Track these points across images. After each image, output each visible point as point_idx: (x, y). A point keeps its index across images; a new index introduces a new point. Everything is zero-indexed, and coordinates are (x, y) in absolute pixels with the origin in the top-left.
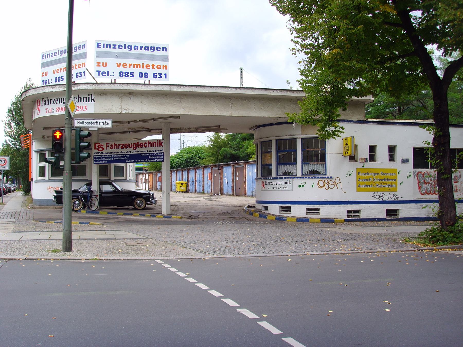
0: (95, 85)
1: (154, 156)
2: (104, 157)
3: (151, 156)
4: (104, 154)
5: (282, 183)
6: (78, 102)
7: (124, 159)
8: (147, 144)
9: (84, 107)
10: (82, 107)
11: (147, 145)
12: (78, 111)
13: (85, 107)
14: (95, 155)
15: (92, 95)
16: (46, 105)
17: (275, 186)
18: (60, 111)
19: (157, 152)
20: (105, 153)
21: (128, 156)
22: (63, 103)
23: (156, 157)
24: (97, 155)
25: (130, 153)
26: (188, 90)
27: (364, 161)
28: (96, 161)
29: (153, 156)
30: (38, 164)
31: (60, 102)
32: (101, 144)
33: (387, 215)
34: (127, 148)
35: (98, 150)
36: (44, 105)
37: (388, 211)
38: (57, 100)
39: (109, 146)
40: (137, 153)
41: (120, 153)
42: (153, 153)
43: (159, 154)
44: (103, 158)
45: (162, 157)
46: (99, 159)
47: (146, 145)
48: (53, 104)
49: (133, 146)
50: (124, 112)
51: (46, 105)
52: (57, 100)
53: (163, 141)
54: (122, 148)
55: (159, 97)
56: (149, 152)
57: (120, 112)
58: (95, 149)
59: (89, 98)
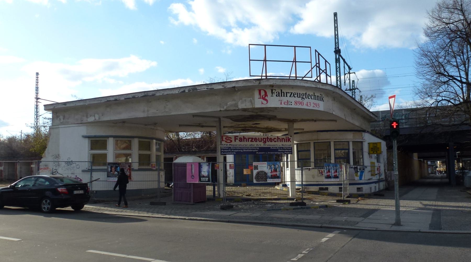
1: (283, 149)
2: (233, 148)
3: (281, 149)
4: (233, 146)
5: (313, 97)
6: (314, 99)
11: (277, 140)
14: (222, 146)
16: (279, 96)
19: (286, 146)
21: (258, 148)
22: (301, 98)
23: (285, 151)
24: (225, 146)
25: (260, 146)
29: (282, 149)
31: (299, 96)
35: (226, 142)
39: (237, 139)
40: (267, 146)
41: (250, 145)
42: (282, 147)
43: (287, 148)
44: (231, 149)
45: (291, 150)
46: (227, 151)
48: (290, 96)
51: (279, 96)
53: (291, 138)
54: (251, 141)
56: (278, 146)
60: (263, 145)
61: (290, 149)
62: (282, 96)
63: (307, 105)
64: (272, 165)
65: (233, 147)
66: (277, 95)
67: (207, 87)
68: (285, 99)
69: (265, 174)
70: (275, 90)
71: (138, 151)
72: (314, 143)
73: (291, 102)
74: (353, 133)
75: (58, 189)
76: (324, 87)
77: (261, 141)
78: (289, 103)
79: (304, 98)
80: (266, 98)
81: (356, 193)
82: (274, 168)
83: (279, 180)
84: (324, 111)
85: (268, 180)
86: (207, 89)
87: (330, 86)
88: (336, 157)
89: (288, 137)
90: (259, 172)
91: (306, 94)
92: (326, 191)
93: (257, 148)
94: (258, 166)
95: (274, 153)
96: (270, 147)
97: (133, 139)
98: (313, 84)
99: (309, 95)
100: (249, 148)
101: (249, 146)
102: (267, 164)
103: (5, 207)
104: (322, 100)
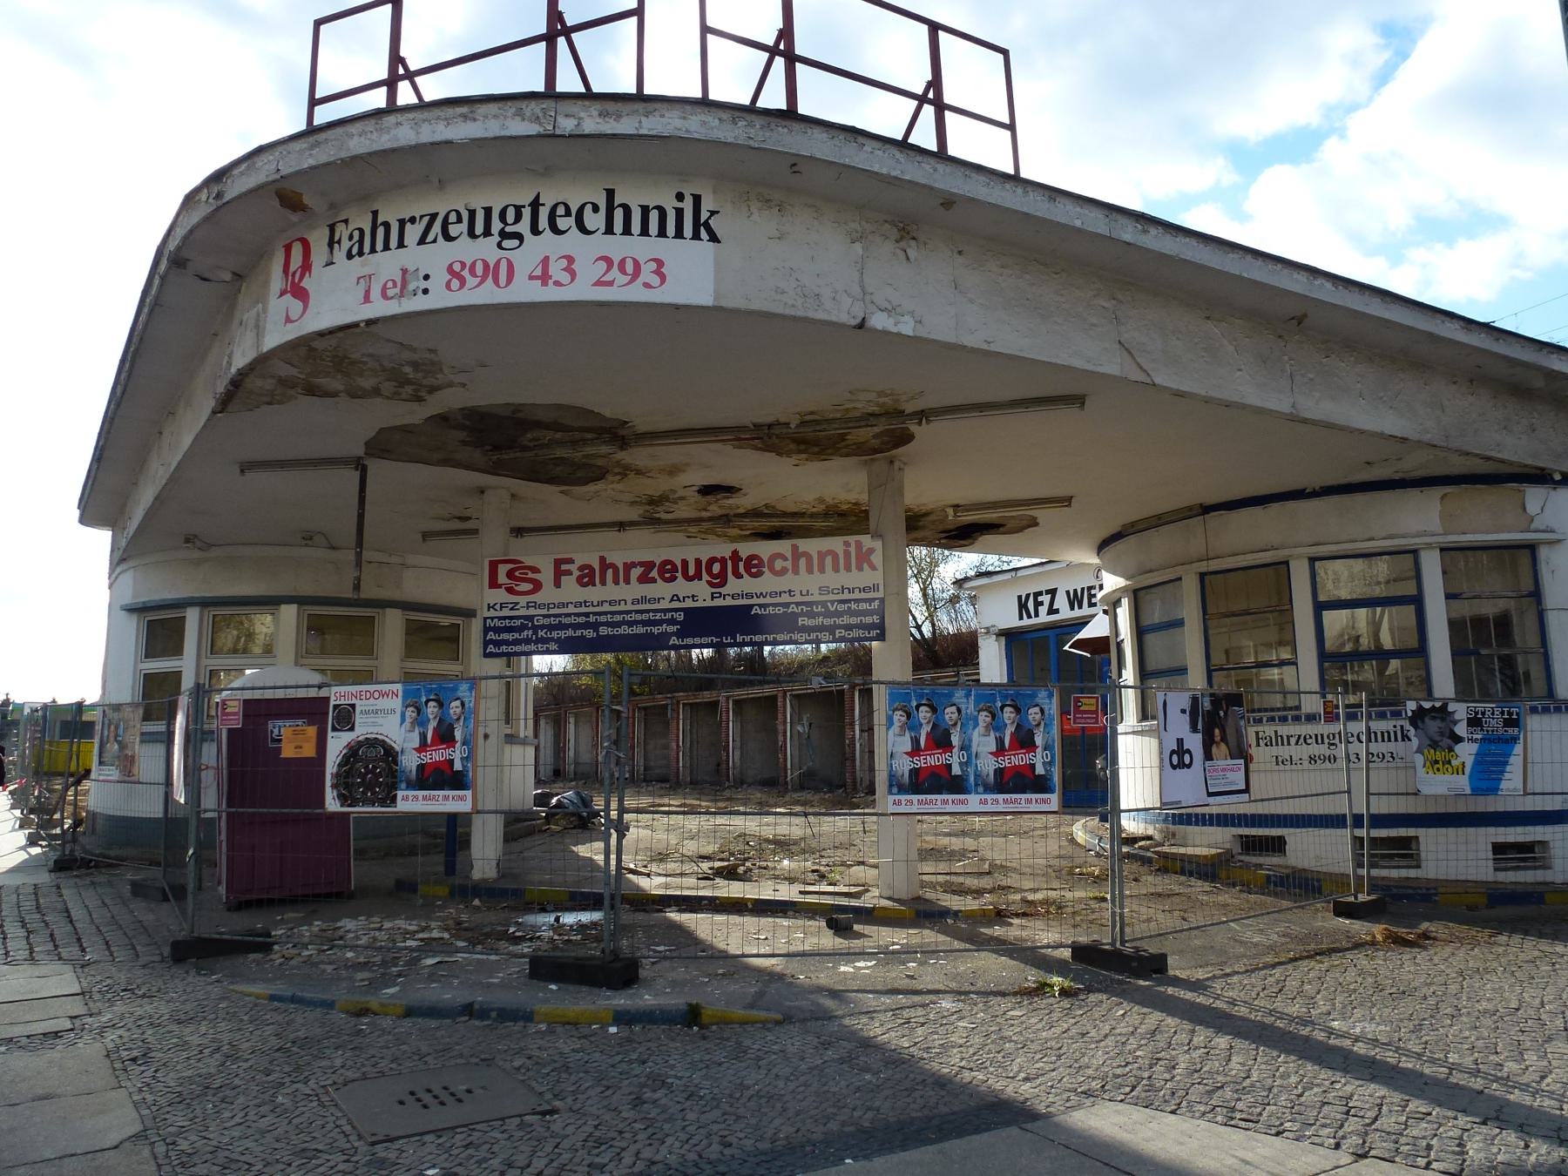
0: (750, 125)
1: (827, 614)
2: (546, 621)
3: (811, 615)
4: (545, 612)
5: (595, 221)
6: (609, 230)
7: (655, 630)
8: (785, 559)
10: (637, 264)
11: (789, 564)
12: (610, 284)
13: (564, 263)
14: (492, 613)
15: (697, 200)
16: (361, 253)
17: (1323, 750)
18: (471, 281)
21: (680, 617)
23: (839, 621)
24: (506, 612)
25: (689, 604)
28: (497, 643)
29: (819, 614)
30: (205, 662)
31: (479, 229)
32: (528, 561)
34: (673, 579)
35: (510, 590)
36: (350, 256)
38: (453, 218)
39: (569, 573)
40: (729, 602)
41: (636, 601)
42: (824, 604)
43: (853, 606)
44: (535, 629)
46: (517, 635)
47: (779, 564)
48: (422, 241)
49: (709, 571)
51: (361, 253)
52: (453, 218)
54: (645, 579)
56: (798, 598)
57: (858, 320)
58: (494, 584)
59: (680, 213)
63: (545, 278)
64: (922, 708)
65: (545, 616)
68: (386, 264)
69: (390, 754)
70: (346, 221)
71: (402, 660)
72: (1202, 576)
76: (626, 126)
77: (698, 576)
78: (411, 287)
79: (519, 237)
81: (1491, 878)
82: (934, 726)
83: (461, 798)
84: (716, 309)
85: (400, 794)
87: (698, 109)
88: (1421, 660)
90: (360, 744)
91: (535, 205)
92: (1275, 860)
93: (676, 615)
94: (353, 706)
96: (752, 606)
97: (380, 611)
98: (519, 114)
99: (561, 210)
100: (627, 618)
101: (629, 607)
102: (400, 694)
104: (703, 229)
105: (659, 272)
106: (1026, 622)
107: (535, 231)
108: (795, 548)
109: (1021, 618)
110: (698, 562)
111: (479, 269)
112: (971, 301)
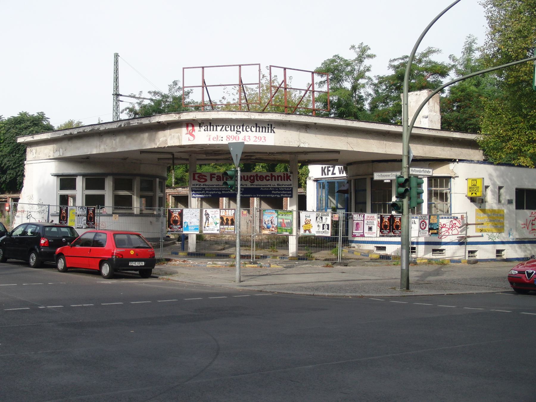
1: (279, 191)
2: (208, 189)
3: (275, 191)
4: (208, 187)
6: (256, 131)
9: (263, 138)
10: (261, 137)
11: (270, 178)
12: (256, 141)
13: (248, 137)
15: (271, 125)
16: (207, 130)
19: (284, 186)
20: (209, 185)
23: (282, 192)
24: (197, 186)
25: (245, 186)
26: (361, 126)
27: (481, 201)
29: (277, 190)
31: (232, 129)
33: (497, 256)
35: (199, 181)
37: (499, 252)
39: (214, 177)
40: (255, 186)
42: (278, 188)
43: (285, 189)
45: (290, 192)
48: (221, 130)
50: (302, 145)
51: (207, 130)
53: (291, 175)
55: (308, 131)
56: (272, 186)
58: (194, 179)
60: (250, 185)
61: (288, 191)
62: (210, 130)
65: (208, 188)
66: (205, 129)
67: (138, 122)
73: (222, 138)
74: (429, 164)
75: (52, 230)
77: (247, 180)
78: (219, 139)
79: (240, 132)
80: (193, 133)
86: (138, 123)
89: (287, 174)
95: (265, 196)
103: (143, 264)
105: (265, 139)
106: (324, 176)
107: (243, 131)
108: (271, 174)
109: (322, 175)
110: (247, 176)
111: (233, 138)
112: (318, 138)
